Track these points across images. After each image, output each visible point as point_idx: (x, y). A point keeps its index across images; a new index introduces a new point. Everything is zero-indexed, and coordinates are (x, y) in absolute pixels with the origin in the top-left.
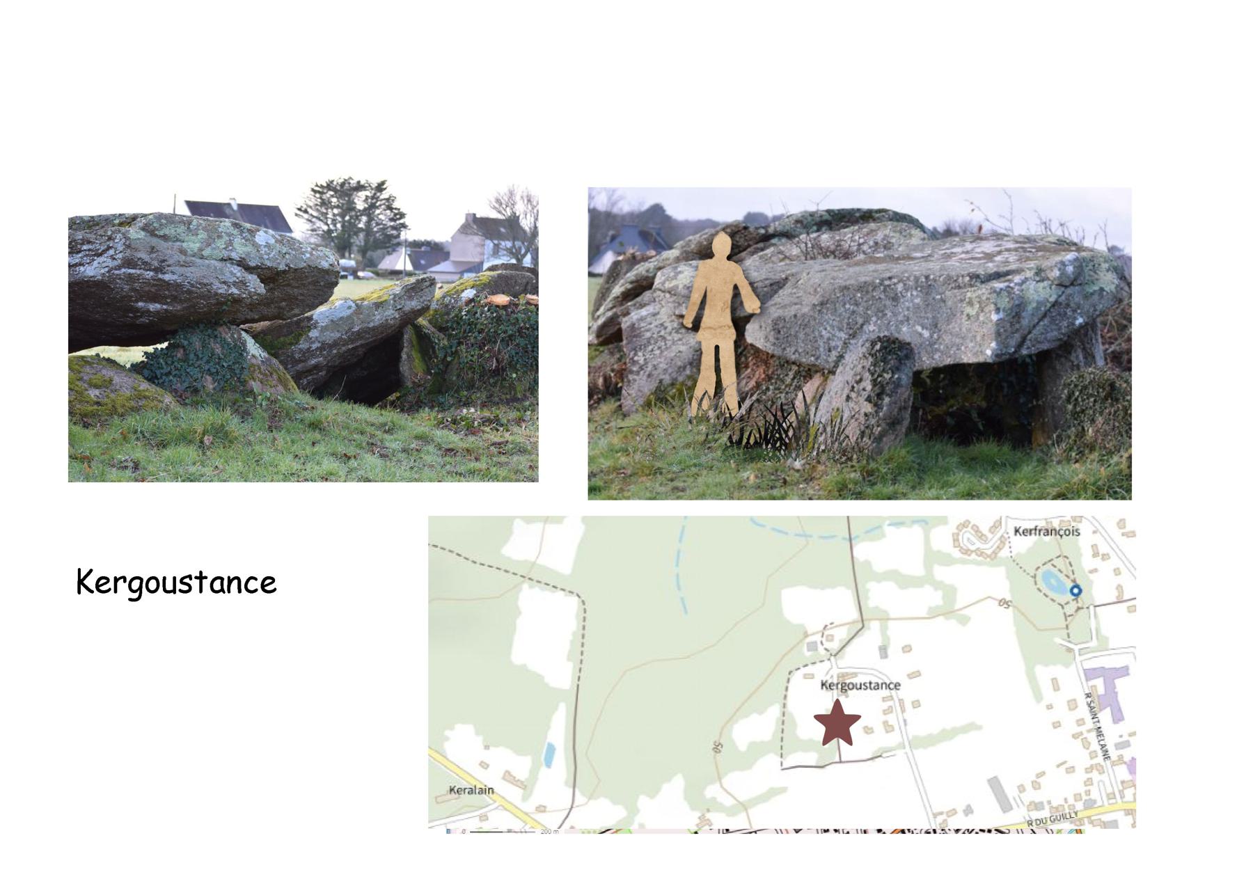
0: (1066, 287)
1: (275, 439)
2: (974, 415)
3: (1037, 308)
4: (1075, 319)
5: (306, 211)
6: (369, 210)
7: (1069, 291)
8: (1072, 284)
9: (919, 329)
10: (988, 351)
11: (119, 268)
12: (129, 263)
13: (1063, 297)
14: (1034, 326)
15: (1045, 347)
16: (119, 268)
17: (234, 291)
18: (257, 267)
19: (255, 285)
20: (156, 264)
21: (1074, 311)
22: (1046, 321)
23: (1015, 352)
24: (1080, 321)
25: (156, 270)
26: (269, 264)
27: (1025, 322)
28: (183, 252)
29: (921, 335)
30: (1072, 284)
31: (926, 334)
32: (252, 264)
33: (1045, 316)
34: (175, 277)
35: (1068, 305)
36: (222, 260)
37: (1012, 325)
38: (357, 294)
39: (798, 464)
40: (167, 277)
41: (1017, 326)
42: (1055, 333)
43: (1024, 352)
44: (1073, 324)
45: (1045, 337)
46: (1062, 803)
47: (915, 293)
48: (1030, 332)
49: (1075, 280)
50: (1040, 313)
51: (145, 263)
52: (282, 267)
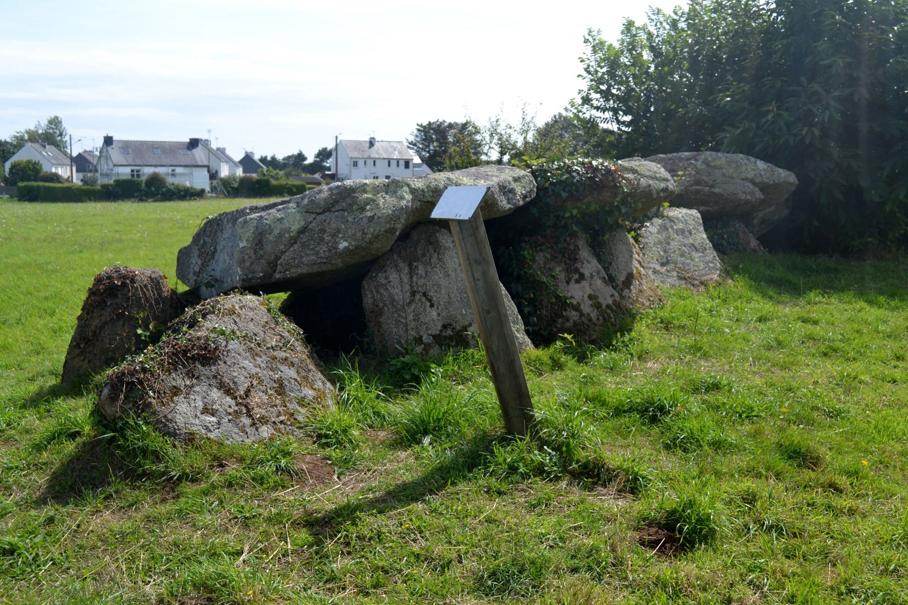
3: (280, 235)
5: (415, 145)
6: (457, 142)
11: (692, 186)
12: (698, 183)
16: (692, 186)
17: (749, 197)
18: (760, 183)
19: (759, 195)
20: (711, 182)
22: (296, 247)
24: (343, 245)
25: (712, 186)
26: (766, 180)
27: (268, 248)
28: (724, 175)
32: (757, 181)
34: (720, 190)
36: (743, 179)
37: (255, 252)
38: (459, 200)
39: (865, 462)
40: (716, 190)
41: (261, 252)
42: (313, 257)
44: (337, 248)
51: (706, 183)
52: (771, 182)
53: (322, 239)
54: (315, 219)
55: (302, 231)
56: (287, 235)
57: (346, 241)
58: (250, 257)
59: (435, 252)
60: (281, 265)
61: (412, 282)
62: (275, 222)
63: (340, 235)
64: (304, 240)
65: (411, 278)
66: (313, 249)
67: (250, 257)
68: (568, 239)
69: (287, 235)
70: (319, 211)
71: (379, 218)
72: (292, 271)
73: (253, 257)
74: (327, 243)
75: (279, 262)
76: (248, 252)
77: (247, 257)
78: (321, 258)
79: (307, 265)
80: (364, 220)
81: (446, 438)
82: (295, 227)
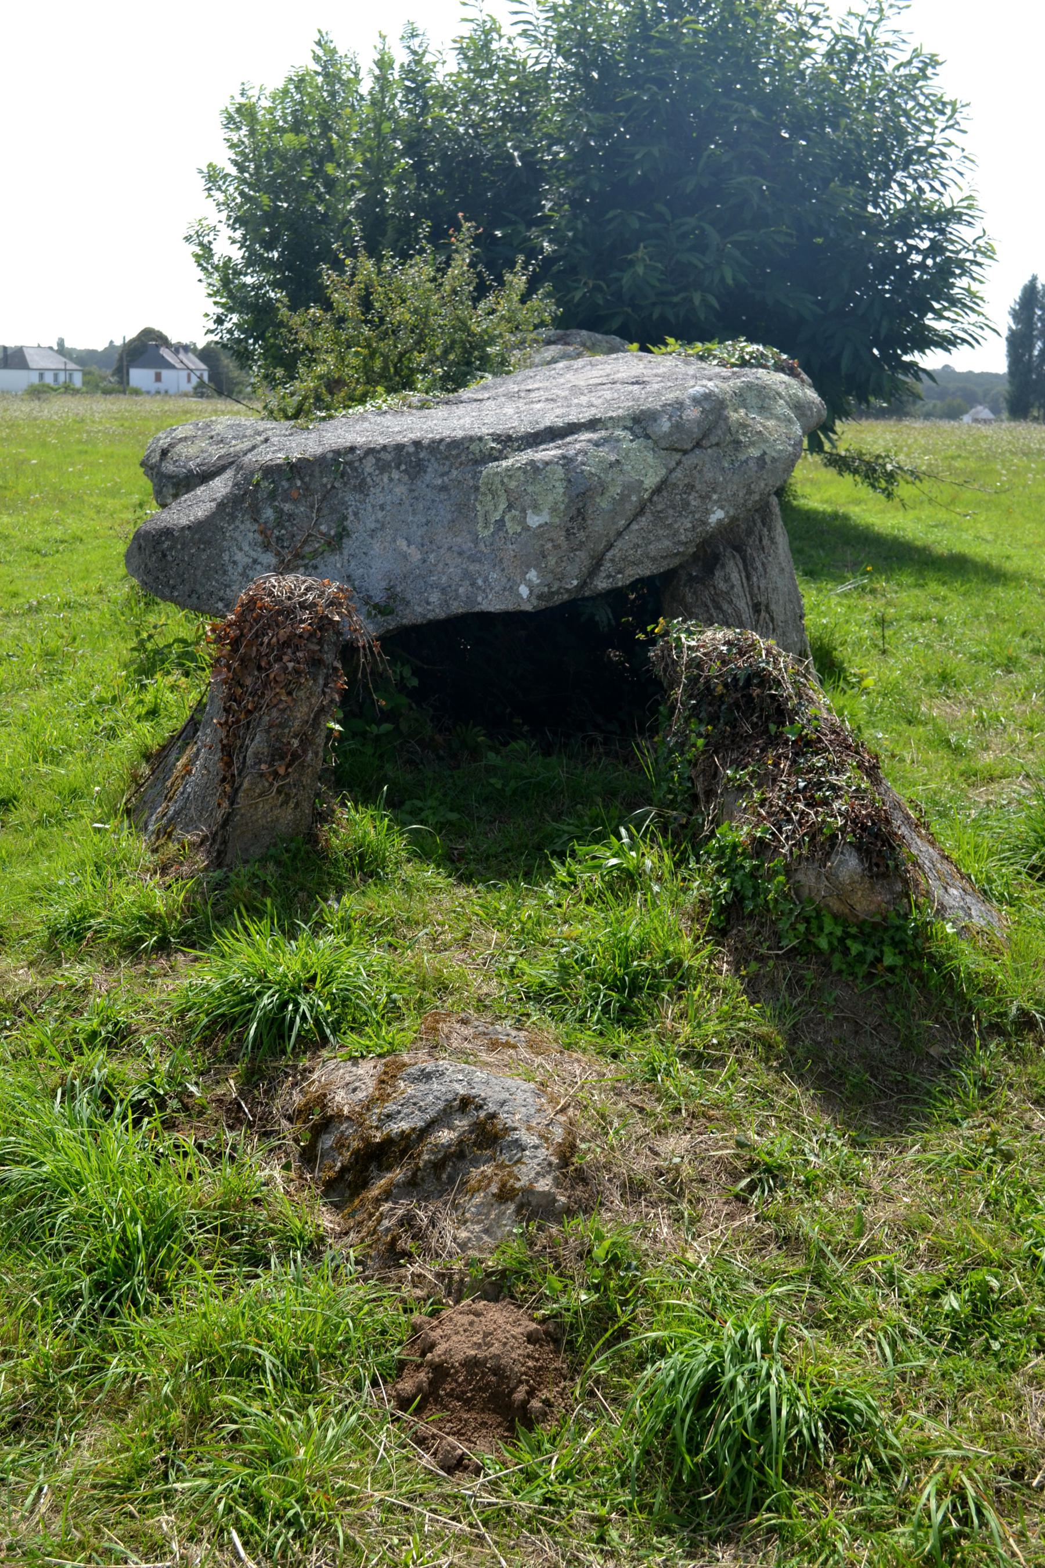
0: (685, 452)
1: (32, 1334)
2: (626, 1381)
3: (624, 498)
4: (708, 512)
7: (689, 460)
8: (698, 445)
9: (402, 544)
10: (525, 592)
13: (678, 474)
14: (620, 534)
15: (647, 570)
21: (705, 497)
22: (643, 521)
23: (583, 585)
24: (717, 515)
27: (598, 525)
29: (405, 557)
30: (698, 445)
31: (415, 555)
33: (641, 511)
35: (690, 487)
41: (582, 535)
42: (667, 543)
43: (602, 584)
44: (705, 523)
45: (637, 555)
46: (204, 284)
47: (395, 475)
48: (610, 546)
49: (705, 436)
50: (630, 508)
53: (686, 504)
54: (679, 463)
55: (658, 490)
56: (634, 498)
57: (722, 508)
58: (557, 547)
59: (764, 525)
60: (612, 561)
61: (751, 586)
62: (606, 471)
63: (715, 497)
64: (659, 507)
65: (748, 578)
66: (670, 526)
67: (557, 547)
68: (380, 515)
69: (634, 498)
70: (689, 446)
71: (774, 460)
72: (627, 573)
73: (565, 545)
74: (693, 513)
75: (609, 555)
76: (554, 535)
77: (549, 545)
78: (680, 543)
79: (654, 559)
80: (751, 464)
81: (410, 928)
82: (651, 481)
